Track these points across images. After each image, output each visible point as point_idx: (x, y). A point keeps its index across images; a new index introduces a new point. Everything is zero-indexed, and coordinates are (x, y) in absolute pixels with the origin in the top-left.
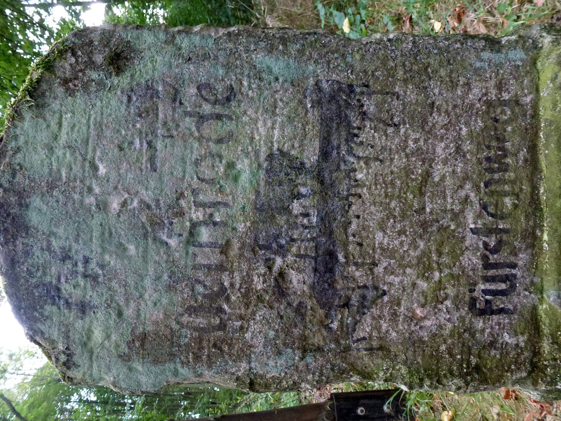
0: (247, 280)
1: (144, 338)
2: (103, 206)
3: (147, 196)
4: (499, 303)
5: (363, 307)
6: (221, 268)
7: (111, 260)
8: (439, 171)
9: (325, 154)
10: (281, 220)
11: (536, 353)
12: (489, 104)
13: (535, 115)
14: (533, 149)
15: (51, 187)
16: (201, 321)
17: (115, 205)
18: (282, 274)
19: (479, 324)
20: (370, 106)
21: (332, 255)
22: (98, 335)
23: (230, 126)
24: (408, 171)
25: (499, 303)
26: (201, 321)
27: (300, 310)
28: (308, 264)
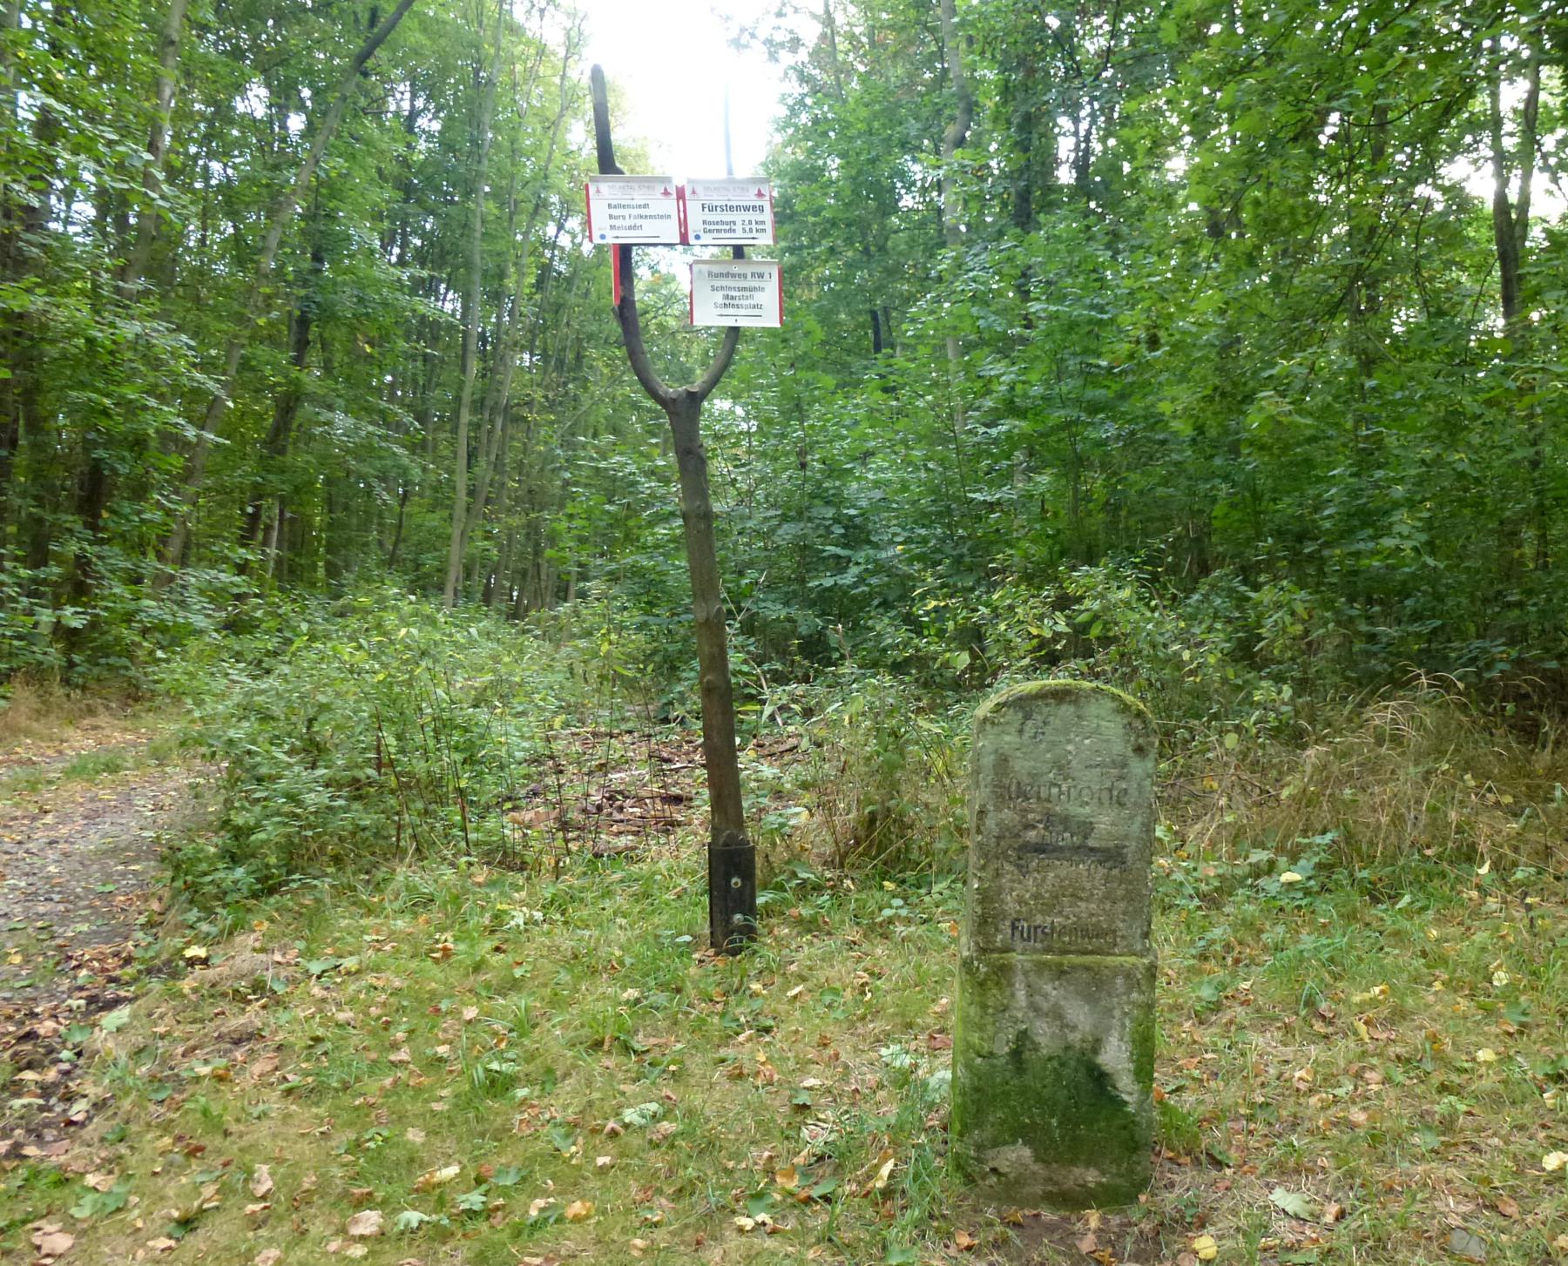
0: (1033, 811)
1: (1006, 760)
2: (1069, 742)
3: (1074, 763)
4: (1017, 934)
5: (1019, 867)
6: (1039, 798)
7: (1043, 746)
8: (1083, 905)
9: (1092, 849)
10: (1061, 828)
11: (992, 951)
12: (1114, 931)
13: (1109, 954)
14: (1092, 953)
15: (1079, 717)
16: (1013, 788)
17: (1070, 748)
18: (1034, 827)
19: (1008, 923)
20: (1115, 872)
21: (1043, 852)
22: (1007, 738)
23: (1107, 803)
24: (1083, 889)
25: (1017, 934)
26: (1013, 788)
27: (1018, 836)
28: (1039, 840)
